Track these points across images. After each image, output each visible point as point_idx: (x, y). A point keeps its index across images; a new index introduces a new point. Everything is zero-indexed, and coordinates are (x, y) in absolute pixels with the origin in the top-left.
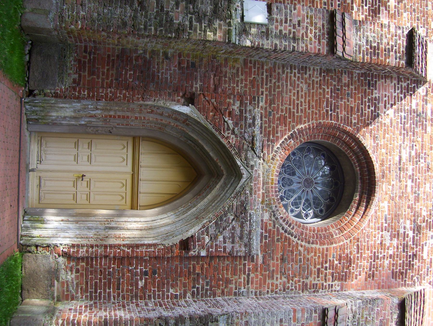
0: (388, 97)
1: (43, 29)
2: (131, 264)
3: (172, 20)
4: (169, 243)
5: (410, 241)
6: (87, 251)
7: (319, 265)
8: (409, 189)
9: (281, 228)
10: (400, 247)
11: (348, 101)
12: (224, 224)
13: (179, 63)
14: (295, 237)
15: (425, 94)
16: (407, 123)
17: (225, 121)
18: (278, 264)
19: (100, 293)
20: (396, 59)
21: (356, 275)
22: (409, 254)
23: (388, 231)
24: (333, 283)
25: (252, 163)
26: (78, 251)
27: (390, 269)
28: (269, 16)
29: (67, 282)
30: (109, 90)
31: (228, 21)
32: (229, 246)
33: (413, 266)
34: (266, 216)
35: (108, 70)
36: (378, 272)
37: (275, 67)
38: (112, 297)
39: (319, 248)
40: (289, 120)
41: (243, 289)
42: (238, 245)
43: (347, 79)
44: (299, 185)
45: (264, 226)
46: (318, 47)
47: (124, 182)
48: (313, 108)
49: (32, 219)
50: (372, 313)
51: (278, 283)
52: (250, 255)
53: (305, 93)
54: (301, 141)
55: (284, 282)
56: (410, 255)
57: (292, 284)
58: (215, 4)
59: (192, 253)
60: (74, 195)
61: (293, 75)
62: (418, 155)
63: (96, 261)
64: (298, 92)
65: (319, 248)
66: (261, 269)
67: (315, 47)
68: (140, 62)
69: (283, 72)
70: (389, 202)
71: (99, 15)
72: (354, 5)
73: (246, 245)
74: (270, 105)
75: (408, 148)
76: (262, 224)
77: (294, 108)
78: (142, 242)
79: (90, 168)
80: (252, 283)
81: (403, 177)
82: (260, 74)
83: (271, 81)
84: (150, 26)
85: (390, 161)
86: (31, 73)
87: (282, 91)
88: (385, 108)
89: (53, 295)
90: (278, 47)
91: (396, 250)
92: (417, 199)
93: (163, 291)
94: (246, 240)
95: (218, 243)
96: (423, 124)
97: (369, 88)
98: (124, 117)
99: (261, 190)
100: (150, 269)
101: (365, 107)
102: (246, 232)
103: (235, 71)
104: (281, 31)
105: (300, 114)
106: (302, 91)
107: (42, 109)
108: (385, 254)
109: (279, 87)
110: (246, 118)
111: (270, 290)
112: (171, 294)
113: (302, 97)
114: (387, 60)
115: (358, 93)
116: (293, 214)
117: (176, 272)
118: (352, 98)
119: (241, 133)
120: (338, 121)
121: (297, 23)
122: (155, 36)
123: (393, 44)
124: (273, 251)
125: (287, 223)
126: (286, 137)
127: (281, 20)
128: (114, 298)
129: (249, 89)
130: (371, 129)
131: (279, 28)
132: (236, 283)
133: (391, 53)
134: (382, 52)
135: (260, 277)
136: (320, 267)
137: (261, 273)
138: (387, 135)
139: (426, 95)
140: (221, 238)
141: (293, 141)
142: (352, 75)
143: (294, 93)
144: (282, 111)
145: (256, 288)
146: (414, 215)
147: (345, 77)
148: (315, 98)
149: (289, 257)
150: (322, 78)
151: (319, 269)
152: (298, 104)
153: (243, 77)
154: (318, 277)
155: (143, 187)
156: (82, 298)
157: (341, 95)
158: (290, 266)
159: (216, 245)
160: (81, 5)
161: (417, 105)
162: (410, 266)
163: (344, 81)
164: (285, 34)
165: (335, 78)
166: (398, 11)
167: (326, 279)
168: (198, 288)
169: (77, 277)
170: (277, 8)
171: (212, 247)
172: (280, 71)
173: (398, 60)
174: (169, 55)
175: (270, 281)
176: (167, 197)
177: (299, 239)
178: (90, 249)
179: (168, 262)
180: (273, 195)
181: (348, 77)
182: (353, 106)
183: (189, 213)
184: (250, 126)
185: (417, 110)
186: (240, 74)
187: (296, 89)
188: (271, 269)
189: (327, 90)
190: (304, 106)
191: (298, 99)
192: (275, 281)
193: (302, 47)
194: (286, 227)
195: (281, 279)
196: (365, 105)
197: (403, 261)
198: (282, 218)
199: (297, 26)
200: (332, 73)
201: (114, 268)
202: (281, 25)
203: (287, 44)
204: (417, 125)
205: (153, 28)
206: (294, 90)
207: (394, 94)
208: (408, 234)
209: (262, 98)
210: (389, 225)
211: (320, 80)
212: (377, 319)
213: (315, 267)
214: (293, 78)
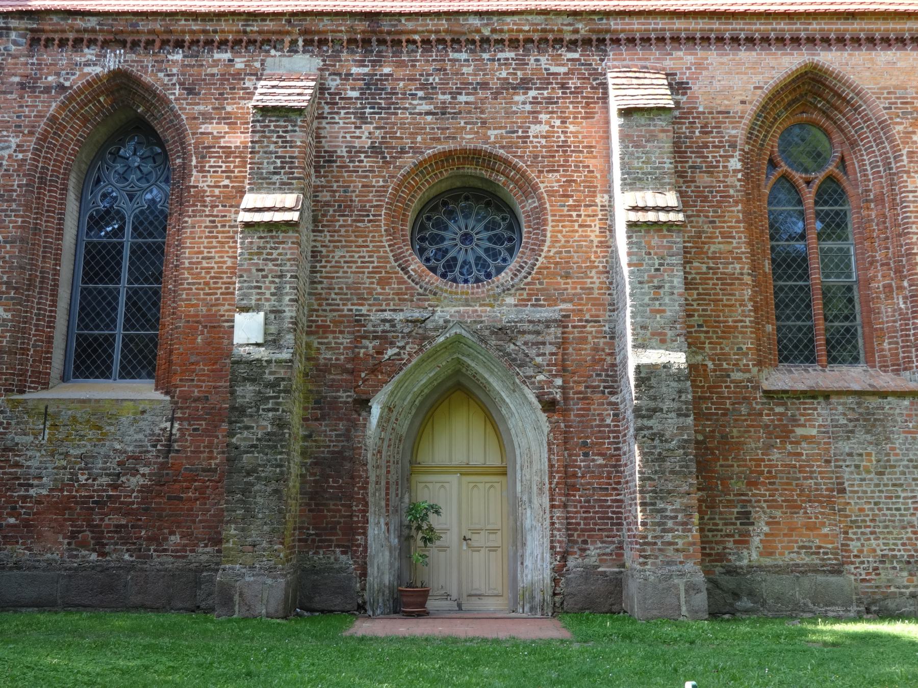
0: (346, 133)
1: (286, 591)
2: (574, 475)
3: (268, 434)
4: (546, 428)
5: (542, 94)
6: (559, 530)
7: (573, 226)
8: (471, 99)
9: (526, 281)
10: (550, 109)
11: (354, 191)
12: (521, 356)
13: (317, 419)
14: (537, 260)
15: (337, 78)
16: (380, 104)
17: (389, 359)
18: (573, 283)
19: (613, 512)
20: (295, 131)
21: (589, 172)
22: (560, 95)
23: (529, 128)
24: (599, 204)
25: (441, 322)
26: (559, 542)
27: (581, 123)
28: (254, 311)
29: (599, 555)
30: (354, 508)
31: (265, 364)
32: (549, 349)
33: (578, 88)
34: (510, 300)
35: (329, 511)
36: (585, 140)
37: (315, 294)
38: (618, 497)
39: (552, 226)
40: (383, 274)
41: (606, 328)
42: (548, 338)
43: (325, 193)
44: (470, 251)
45: (522, 303)
46: (290, 245)
47: (471, 485)
48: (366, 241)
49: (521, 603)
50: (636, 155)
51: (597, 281)
52: (560, 321)
53: (348, 252)
54: (411, 255)
55: (597, 273)
56: (563, 93)
57: (600, 262)
58: (244, 381)
59: (558, 397)
60: (490, 551)
61: (324, 270)
62: (423, 87)
63: (572, 518)
64: (345, 262)
65: (552, 226)
66: (580, 305)
67: (290, 248)
68: (317, 470)
69: (321, 282)
70: (489, 128)
71: (266, 524)
72: (222, 184)
73: (548, 327)
74: (365, 299)
75: (415, 102)
76: (521, 305)
77: (368, 267)
78: (546, 460)
79: (455, 530)
80: (598, 316)
81: (455, 108)
82: (325, 313)
83: (333, 300)
84: (276, 460)
85: (433, 129)
86: (336, 608)
87: (346, 283)
88: (360, 137)
89: (617, 573)
90: (293, 297)
91: (555, 116)
92: (484, 85)
93: (609, 432)
94: (540, 327)
95: (545, 363)
96: (381, 80)
97: (335, 161)
98: (387, 489)
99: (476, 308)
100: (580, 449)
101: (361, 167)
102: (530, 327)
103: (323, 347)
104: (273, 294)
105: (375, 259)
106: (344, 257)
107: (381, 594)
108: (560, 130)
109: (341, 289)
110: (383, 331)
111: (608, 292)
112: (612, 421)
113: (352, 257)
114: (299, 144)
115: (343, 177)
116: (508, 258)
117: (583, 416)
118: (349, 187)
119: (403, 337)
120: (381, 206)
121: (260, 274)
122: (288, 454)
123: (275, 135)
124: (555, 290)
125: (519, 271)
126: (406, 277)
127: (258, 294)
128: (618, 495)
129: (345, 327)
130: (391, 157)
131: (268, 296)
132: (597, 338)
133: (288, 139)
134: (287, 152)
135: (589, 307)
136: (576, 224)
137: (584, 305)
138: (398, 135)
139: (340, 74)
140: (539, 360)
141: (412, 267)
142: (318, 186)
143: (348, 267)
144: (372, 283)
145: (605, 310)
146: (507, 89)
147: (322, 196)
148: (353, 238)
149: (564, 268)
150: (326, 229)
151: (580, 226)
152: (362, 262)
153: (331, 336)
154: (590, 226)
155: (477, 459)
156: (620, 536)
157: (347, 201)
158: (575, 266)
159: (548, 365)
160: (254, 546)
161: (353, 89)
162: (578, 93)
163: (328, 198)
164: (275, 288)
165: (325, 211)
166: (224, 118)
167: (593, 216)
168: (605, 387)
169: (594, 543)
170: (242, 300)
171: (551, 371)
172: (319, 286)
173: (297, 129)
174: (306, 433)
175: (596, 292)
176: (490, 429)
177: (540, 256)
178: (557, 526)
179: (570, 427)
180: (483, 292)
181: (322, 191)
182: (360, 185)
183: (507, 400)
184: (394, 326)
185: (362, 89)
186: (326, 341)
187: (343, 264)
188: (579, 291)
189: (341, 223)
190: (365, 254)
191: (356, 262)
192: (596, 286)
193: (291, 265)
194: (523, 274)
195: (592, 278)
196: (358, 167)
197: (570, 103)
198: (512, 279)
199: (264, 273)
200: (317, 215)
201: (580, 496)
202: (264, 294)
203: (288, 286)
204: (383, 89)
205: (279, 457)
206: (343, 267)
207: (342, 125)
208: (533, 98)
209: (357, 310)
210: (520, 127)
211: (329, 232)
212: (645, 147)
213: (577, 231)
214: (328, 269)
